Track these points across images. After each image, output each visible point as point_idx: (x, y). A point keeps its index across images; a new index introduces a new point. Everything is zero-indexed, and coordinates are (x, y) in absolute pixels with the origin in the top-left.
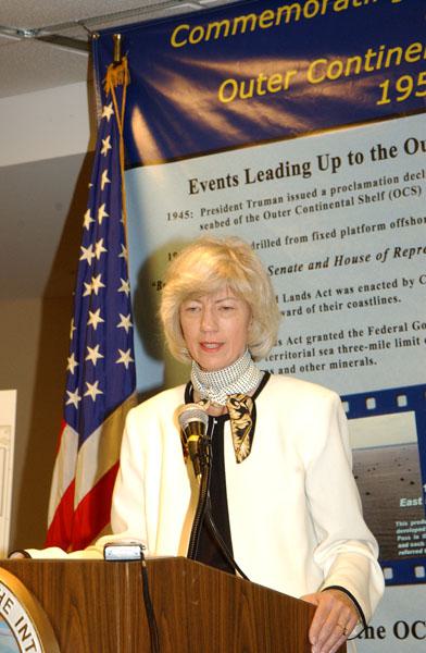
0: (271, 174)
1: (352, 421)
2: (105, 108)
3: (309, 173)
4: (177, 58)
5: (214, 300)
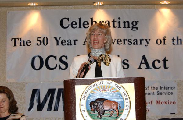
0: (137, 41)
1: (32, 90)
2: (94, 62)
3: (137, 28)
4: (85, 71)
5: (23, 98)
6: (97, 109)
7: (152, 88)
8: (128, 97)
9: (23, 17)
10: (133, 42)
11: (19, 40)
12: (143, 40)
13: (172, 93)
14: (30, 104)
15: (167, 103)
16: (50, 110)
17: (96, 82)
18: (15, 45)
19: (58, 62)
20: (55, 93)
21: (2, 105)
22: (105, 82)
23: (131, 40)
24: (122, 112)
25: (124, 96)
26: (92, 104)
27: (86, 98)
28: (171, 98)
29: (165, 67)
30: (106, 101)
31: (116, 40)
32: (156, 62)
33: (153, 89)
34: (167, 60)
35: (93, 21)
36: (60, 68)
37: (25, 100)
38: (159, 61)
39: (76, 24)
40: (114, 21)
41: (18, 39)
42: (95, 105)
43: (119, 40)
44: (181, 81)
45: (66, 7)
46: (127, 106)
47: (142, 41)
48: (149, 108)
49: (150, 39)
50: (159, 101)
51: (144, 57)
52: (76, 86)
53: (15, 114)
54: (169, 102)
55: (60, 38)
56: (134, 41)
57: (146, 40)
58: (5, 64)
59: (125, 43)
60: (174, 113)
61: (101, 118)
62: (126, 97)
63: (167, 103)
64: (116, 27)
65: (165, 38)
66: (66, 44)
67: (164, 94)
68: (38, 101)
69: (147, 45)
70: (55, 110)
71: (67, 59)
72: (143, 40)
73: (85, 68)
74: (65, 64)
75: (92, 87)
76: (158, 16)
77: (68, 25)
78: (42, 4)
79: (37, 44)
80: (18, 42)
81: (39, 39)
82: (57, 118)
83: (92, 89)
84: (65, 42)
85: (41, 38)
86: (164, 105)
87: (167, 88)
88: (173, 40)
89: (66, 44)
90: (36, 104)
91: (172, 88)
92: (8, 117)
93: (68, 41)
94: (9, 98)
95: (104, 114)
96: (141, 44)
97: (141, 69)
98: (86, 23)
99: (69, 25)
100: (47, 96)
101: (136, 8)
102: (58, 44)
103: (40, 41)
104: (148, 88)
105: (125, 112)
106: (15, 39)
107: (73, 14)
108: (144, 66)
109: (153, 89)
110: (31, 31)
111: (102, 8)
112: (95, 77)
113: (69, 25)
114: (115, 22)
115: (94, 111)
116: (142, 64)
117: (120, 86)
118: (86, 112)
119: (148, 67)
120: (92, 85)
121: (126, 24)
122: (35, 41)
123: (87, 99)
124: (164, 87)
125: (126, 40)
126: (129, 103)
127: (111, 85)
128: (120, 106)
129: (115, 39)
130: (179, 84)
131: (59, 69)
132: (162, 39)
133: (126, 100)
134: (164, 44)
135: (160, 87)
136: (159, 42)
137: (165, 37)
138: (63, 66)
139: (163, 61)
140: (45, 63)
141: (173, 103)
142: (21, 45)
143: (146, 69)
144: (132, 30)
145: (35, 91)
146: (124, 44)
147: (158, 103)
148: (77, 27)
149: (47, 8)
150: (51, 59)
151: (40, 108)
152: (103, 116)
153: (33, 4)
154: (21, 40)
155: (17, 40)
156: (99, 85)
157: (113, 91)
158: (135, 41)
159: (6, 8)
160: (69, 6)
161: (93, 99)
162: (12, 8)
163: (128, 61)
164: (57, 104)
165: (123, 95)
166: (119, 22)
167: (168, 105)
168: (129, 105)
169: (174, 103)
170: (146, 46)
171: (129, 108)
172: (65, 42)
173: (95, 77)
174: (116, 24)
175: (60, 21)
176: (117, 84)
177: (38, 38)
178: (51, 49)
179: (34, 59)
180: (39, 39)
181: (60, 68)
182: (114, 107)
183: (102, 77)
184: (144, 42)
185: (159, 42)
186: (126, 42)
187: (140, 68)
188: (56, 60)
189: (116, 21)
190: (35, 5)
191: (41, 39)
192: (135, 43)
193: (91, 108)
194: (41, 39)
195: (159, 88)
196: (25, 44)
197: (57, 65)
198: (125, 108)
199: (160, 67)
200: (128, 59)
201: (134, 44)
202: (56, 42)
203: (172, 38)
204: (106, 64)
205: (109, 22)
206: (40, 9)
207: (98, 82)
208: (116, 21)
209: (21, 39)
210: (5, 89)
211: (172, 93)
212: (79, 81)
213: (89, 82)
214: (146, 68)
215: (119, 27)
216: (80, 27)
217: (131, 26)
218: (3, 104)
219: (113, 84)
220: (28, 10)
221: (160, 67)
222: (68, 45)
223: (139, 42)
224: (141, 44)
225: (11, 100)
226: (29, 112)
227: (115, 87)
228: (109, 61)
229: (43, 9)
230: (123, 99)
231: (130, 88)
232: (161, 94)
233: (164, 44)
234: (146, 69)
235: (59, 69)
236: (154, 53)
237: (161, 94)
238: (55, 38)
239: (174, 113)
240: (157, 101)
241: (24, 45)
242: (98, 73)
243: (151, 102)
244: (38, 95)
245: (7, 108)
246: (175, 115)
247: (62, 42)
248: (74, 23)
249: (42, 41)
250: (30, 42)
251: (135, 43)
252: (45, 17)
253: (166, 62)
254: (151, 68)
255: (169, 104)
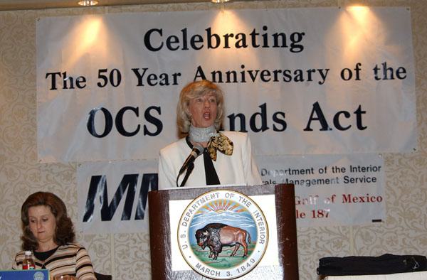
3: (302, 48)
6: (209, 243)
7: (333, 168)
8: (264, 221)
9: (68, 28)
10: (293, 76)
11: (62, 76)
12: (314, 71)
13: (374, 180)
14: (87, 206)
15: (364, 199)
16: (127, 217)
17: (206, 195)
18: (54, 88)
19: (141, 120)
20: (138, 182)
21: (42, 227)
22: (222, 195)
23: (290, 71)
24: (253, 247)
25: (256, 220)
26: (199, 234)
27: (188, 223)
28: (372, 189)
29: (360, 127)
30: (225, 227)
31: (259, 73)
32: (342, 116)
33: (335, 170)
34: (364, 112)
35: (212, 33)
36: (146, 132)
37: (76, 198)
38: (347, 115)
39: (177, 41)
40: (254, 35)
41: (59, 74)
42: (205, 236)
43: (265, 73)
44: (392, 154)
45: (155, 6)
46: (263, 237)
47: (312, 73)
48: (329, 210)
49: (327, 70)
50: (349, 196)
51: (316, 107)
52: (170, 201)
53: (66, 246)
54: (368, 198)
55: (145, 70)
56: (295, 73)
57: (320, 71)
58: (35, 126)
59: (278, 79)
60: (380, 221)
61: (215, 258)
62: (260, 221)
63: (365, 199)
64: (259, 46)
65: (359, 67)
66: (157, 83)
67: (358, 180)
68: (102, 201)
69: (322, 81)
70: (137, 218)
71: (160, 113)
72: (314, 71)
73: (188, 166)
74: (154, 124)
75: (200, 203)
76: (344, 21)
77: (160, 45)
78: (106, 2)
79: (99, 85)
80: (59, 80)
81: (102, 74)
82: (142, 234)
83: (199, 207)
84: (156, 78)
85: (105, 71)
86: (359, 205)
87: (363, 169)
88: (376, 70)
89: (158, 84)
90: (98, 206)
91: (375, 169)
92: (54, 251)
93: (161, 77)
94: (56, 215)
95: (220, 251)
96: (310, 79)
97: (312, 130)
98: (197, 39)
99: (163, 43)
100: (121, 188)
101: (299, 7)
102: (140, 84)
103: (105, 78)
104: (326, 169)
105: (259, 247)
106: (54, 75)
107: (171, 20)
108: (316, 125)
109: (335, 170)
110: (86, 57)
111: (230, 8)
112: (207, 184)
113: (163, 43)
114: (257, 36)
115: (203, 246)
116: (312, 122)
117: (249, 201)
118: (189, 248)
119: (325, 127)
120: (198, 199)
121: (279, 40)
122: (93, 79)
123: (191, 225)
124: (359, 167)
125: (280, 71)
126: (265, 231)
127: (232, 199)
128: (249, 237)
129: (257, 71)
130: (389, 161)
131: (145, 134)
132: (353, 68)
133: (261, 226)
134: (358, 78)
135: (351, 167)
136: (347, 74)
137: (360, 64)
138: (152, 128)
139: (355, 115)
140: (114, 122)
141: (378, 200)
142: (65, 87)
143: (321, 130)
144: (291, 50)
145: (95, 180)
146: (276, 80)
147: (346, 200)
148: (178, 47)
149: (117, 9)
150: (127, 114)
151: (107, 214)
152: (220, 254)
153: (88, 2)
154: (65, 77)
155: (57, 76)
156: (211, 200)
157: (236, 209)
158: (298, 73)
159: (34, 11)
160: (161, 5)
161: (200, 225)
162: (45, 11)
163: (283, 114)
164: (141, 206)
165: (255, 217)
166: (265, 36)
167: (366, 203)
168: (266, 235)
169: (379, 199)
170: (320, 83)
171: (265, 239)
172: (156, 78)
173: (207, 184)
174: (259, 40)
175: (144, 35)
176: (244, 197)
177: (100, 71)
178: (127, 94)
179: (92, 114)
180: (102, 74)
181: (146, 132)
182: (241, 237)
183: (219, 183)
184: (316, 76)
185: (347, 74)
186: (280, 76)
187: (308, 129)
188: (138, 116)
189: (258, 34)
190: (92, 4)
191: (107, 75)
192: (298, 78)
193: (198, 242)
194: (107, 75)
195: (348, 169)
196: (75, 85)
197: (139, 126)
198: (259, 241)
199: (350, 126)
200: (282, 111)
201: (296, 80)
202: (136, 80)
203: (374, 67)
204: (226, 152)
205: (244, 36)
206: (104, 12)
207: (209, 195)
208: (258, 34)
209: (65, 74)
210: (49, 198)
211: (374, 180)
212: (182, 192)
213: (195, 194)
214: (321, 127)
215: (266, 45)
216: (185, 48)
217: (289, 42)
218: (43, 225)
219: (236, 197)
220: (78, 15)
221: (350, 126)
222: (161, 84)
223: (305, 76)
224: (310, 79)
225: (58, 219)
226: (85, 223)
227: (240, 203)
228: (230, 147)
229: (109, 12)
230: (254, 223)
231: (268, 203)
232: (352, 180)
233: (358, 78)
234: (321, 130)
235: (145, 134)
236: (337, 97)
237: (352, 180)
238: (136, 71)
239: (380, 221)
240: (344, 196)
241: (72, 87)
242: (212, 178)
243: (333, 198)
244: (103, 188)
245: (51, 235)
246: (382, 223)
247: (149, 80)
248: (173, 40)
249: (109, 78)
250: (84, 80)
251: (298, 78)
252: (113, 27)
253: (362, 115)
254: (331, 129)
255: (368, 201)
